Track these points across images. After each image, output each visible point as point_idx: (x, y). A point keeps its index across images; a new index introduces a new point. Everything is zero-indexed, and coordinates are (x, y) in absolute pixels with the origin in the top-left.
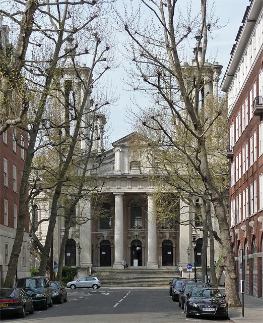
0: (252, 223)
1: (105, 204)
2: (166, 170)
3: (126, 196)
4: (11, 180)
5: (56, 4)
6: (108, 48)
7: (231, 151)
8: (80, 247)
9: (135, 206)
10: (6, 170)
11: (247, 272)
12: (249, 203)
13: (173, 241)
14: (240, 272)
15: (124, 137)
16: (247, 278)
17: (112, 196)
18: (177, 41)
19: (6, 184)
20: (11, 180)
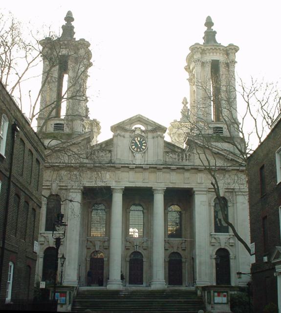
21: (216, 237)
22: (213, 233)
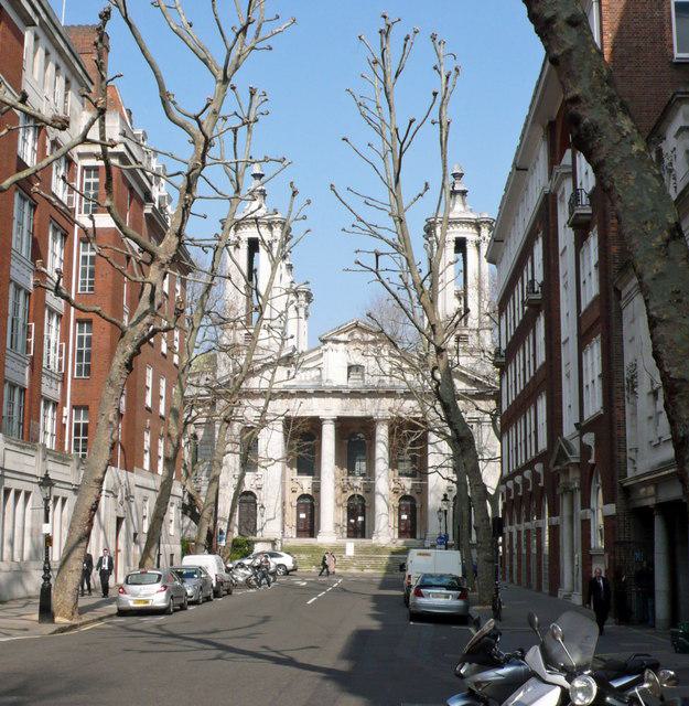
0: (527, 474)
1: (303, 435)
2: (405, 380)
3: (343, 424)
4: (157, 397)
5: (103, 138)
6: (309, 202)
7: (538, 292)
8: (262, 507)
9: (356, 437)
10: (149, 383)
11: (524, 551)
12: (516, 448)
13: (416, 497)
14: (508, 567)
16: (524, 559)
17: (315, 424)
18: (406, 202)
19: (149, 402)
20: (157, 397)
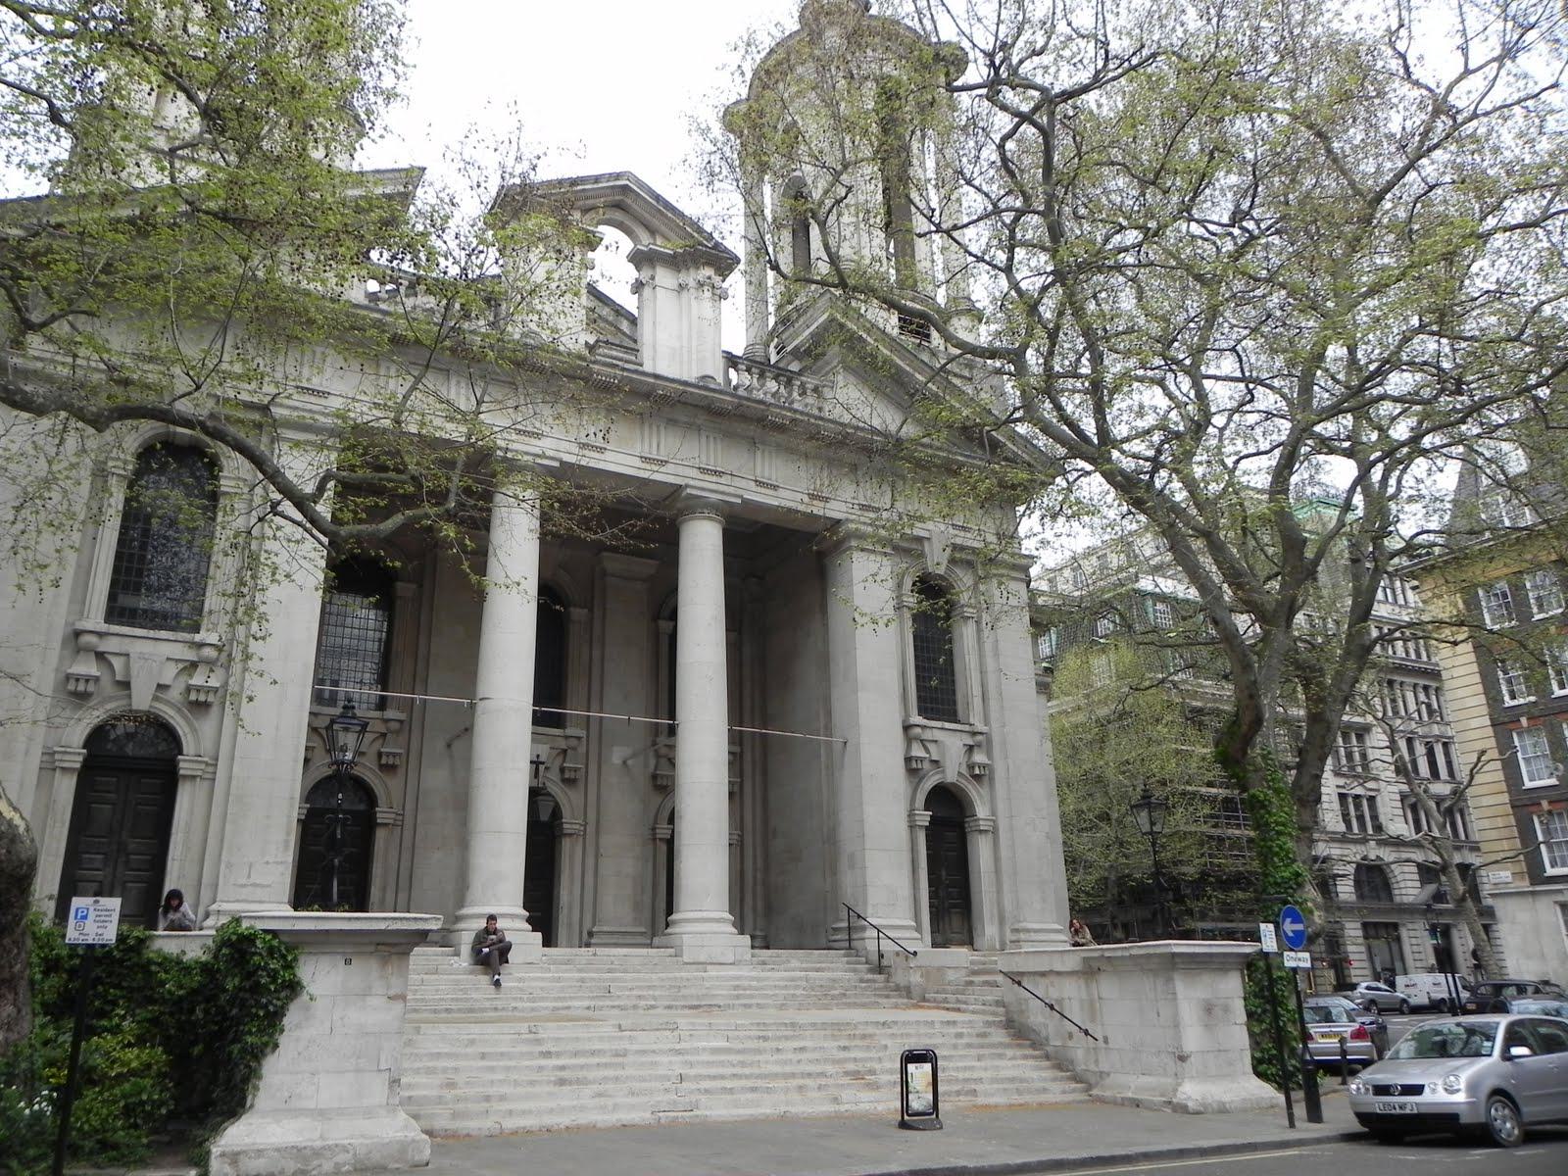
15: (574, 182)
21: (109, 645)
22: (95, 620)
